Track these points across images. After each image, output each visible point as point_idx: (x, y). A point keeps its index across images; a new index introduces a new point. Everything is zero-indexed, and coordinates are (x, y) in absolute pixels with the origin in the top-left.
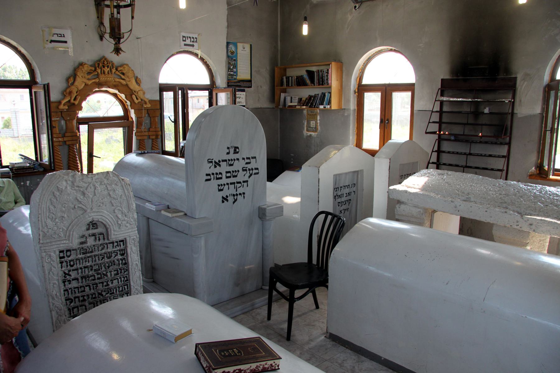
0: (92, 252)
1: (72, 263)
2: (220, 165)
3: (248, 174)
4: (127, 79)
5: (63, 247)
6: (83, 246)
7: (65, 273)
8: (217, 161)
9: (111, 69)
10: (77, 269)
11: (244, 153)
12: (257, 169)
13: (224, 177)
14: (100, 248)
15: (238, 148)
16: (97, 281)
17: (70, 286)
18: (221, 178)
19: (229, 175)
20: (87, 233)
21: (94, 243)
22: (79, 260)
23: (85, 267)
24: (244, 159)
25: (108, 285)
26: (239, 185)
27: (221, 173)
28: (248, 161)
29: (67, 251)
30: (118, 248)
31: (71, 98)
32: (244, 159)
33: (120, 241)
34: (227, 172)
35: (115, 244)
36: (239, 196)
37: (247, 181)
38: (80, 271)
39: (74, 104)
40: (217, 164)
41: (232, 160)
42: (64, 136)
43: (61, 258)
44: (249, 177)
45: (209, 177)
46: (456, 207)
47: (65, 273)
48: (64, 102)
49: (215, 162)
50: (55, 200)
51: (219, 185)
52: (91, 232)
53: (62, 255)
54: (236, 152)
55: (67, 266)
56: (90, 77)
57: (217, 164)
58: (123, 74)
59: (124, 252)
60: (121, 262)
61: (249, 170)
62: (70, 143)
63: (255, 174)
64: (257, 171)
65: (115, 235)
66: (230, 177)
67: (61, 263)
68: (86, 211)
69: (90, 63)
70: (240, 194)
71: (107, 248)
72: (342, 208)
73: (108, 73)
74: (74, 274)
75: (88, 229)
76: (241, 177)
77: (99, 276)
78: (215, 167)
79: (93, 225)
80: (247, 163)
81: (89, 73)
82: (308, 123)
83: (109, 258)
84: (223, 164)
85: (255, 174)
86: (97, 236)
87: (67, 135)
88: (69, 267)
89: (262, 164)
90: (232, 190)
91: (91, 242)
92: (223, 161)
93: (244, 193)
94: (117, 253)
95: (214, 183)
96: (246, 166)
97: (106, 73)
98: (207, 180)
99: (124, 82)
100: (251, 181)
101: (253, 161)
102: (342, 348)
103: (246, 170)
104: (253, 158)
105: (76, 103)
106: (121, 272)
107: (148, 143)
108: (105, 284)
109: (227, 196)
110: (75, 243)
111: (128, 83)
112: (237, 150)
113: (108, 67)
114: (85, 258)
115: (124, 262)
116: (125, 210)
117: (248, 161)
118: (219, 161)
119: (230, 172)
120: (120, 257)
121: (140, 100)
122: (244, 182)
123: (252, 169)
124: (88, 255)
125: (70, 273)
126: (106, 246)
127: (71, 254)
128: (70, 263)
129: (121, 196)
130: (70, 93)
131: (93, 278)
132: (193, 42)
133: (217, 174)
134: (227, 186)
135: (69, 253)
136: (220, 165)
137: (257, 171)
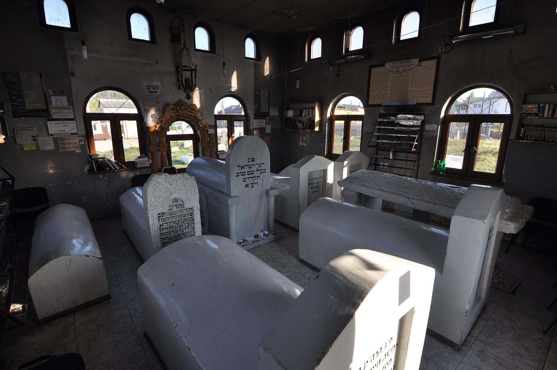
3: (260, 172)
10: (167, 223)
13: (246, 174)
20: (172, 204)
40: (243, 167)
42: (159, 146)
52: (175, 204)
54: (253, 161)
56: (174, 111)
57: (243, 167)
58: (193, 110)
59: (192, 214)
65: (188, 205)
68: (172, 193)
69: (174, 103)
74: (165, 226)
76: (256, 174)
79: (176, 200)
81: (173, 110)
82: (302, 139)
89: (267, 166)
91: (175, 209)
95: (241, 178)
100: (261, 176)
102: (305, 267)
105: (165, 127)
107: (208, 151)
110: (166, 210)
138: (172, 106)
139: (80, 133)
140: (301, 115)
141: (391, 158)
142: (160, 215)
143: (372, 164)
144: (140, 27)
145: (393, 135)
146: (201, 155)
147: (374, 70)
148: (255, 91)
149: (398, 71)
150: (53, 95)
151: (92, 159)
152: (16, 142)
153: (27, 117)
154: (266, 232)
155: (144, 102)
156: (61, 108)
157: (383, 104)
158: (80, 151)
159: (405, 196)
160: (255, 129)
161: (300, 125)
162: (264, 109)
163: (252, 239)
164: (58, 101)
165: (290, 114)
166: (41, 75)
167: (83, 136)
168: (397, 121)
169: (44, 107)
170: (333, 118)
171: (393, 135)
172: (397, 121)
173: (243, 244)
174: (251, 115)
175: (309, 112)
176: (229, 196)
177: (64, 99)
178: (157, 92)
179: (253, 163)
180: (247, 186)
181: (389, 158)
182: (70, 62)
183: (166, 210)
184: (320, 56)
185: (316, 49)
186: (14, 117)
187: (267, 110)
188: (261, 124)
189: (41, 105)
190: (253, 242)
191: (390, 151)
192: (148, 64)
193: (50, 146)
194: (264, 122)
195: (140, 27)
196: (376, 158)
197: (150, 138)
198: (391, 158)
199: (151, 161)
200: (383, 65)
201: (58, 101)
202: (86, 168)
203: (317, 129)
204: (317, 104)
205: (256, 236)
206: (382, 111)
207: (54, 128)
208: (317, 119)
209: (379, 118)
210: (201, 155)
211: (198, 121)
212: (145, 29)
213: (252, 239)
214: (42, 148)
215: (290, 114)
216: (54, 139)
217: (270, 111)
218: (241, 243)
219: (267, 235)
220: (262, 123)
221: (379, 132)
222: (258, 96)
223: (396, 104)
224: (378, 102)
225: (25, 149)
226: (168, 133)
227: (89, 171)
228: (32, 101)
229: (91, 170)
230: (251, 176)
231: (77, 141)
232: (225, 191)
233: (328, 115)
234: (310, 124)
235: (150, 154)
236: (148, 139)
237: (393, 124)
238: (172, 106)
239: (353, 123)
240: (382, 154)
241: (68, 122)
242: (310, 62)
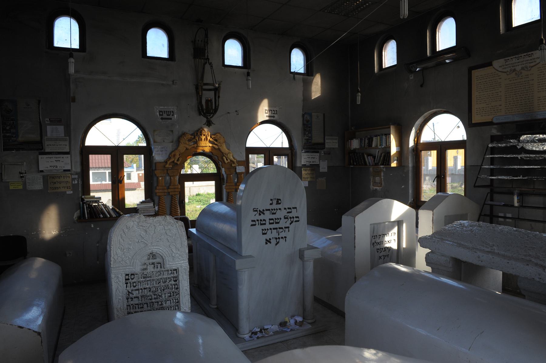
0: (150, 277)
1: (135, 285)
2: (264, 214)
3: (289, 221)
10: (138, 290)
11: (286, 204)
12: (298, 217)
13: (267, 223)
15: (280, 200)
16: (153, 300)
17: (132, 302)
18: (265, 224)
20: (147, 262)
21: (152, 270)
23: (144, 289)
24: (285, 209)
25: (162, 304)
27: (264, 220)
28: (290, 210)
29: (132, 275)
32: (285, 209)
34: (270, 219)
37: (288, 227)
38: (141, 291)
39: (177, 164)
42: (168, 188)
43: (126, 280)
44: (290, 224)
45: (254, 223)
46: (479, 257)
51: (263, 230)
52: (151, 261)
53: (127, 277)
54: (278, 203)
57: (262, 212)
59: (176, 279)
60: (174, 287)
61: (291, 218)
62: (173, 193)
63: (296, 221)
64: (297, 219)
66: (273, 223)
67: (127, 283)
69: (191, 133)
70: (282, 238)
72: (381, 254)
74: (135, 293)
75: (149, 259)
76: (283, 224)
77: (156, 296)
78: (260, 215)
79: (153, 255)
80: (288, 212)
85: (296, 221)
87: (170, 187)
91: (150, 268)
92: (267, 210)
93: (285, 237)
95: (259, 228)
96: (288, 214)
98: (252, 225)
100: (292, 227)
101: (293, 210)
103: (287, 218)
104: (293, 208)
105: (178, 163)
106: (173, 295)
108: (160, 303)
109: (270, 239)
111: (220, 147)
112: (280, 202)
115: (176, 287)
117: (290, 210)
118: (263, 210)
119: (272, 219)
120: (173, 283)
121: (229, 161)
122: (285, 228)
123: (293, 218)
130: (174, 155)
131: (150, 297)
132: (274, 114)
133: (261, 220)
135: (132, 277)
136: (264, 214)
137: (297, 219)
138: (190, 136)
139: (73, 169)
140: (370, 145)
141: (516, 204)
142: (129, 277)
143: (485, 215)
144: (157, 44)
145: (516, 167)
146: (225, 200)
147: (476, 73)
148: (303, 115)
149: (515, 70)
150: (50, 125)
151: (83, 203)
152: (2, 180)
153: (18, 149)
154: (299, 319)
155: (154, 131)
156: (56, 139)
157: (495, 121)
158: (72, 192)
159: (536, 265)
160: (304, 166)
161: (369, 160)
162: (317, 138)
163: (275, 328)
164: (54, 131)
165: (355, 144)
166: (39, 101)
167: (77, 174)
168: (521, 145)
169: (38, 139)
170: (420, 147)
171: (516, 167)
172: (521, 145)
173: (259, 335)
174: (298, 146)
175: (381, 140)
176: (238, 254)
177: (61, 128)
178: (171, 119)
180: (268, 241)
181: (513, 206)
182: (72, 86)
183: (137, 269)
184: (395, 63)
185: (390, 56)
186: (5, 150)
187: (321, 141)
188: (313, 160)
189: (35, 137)
190: (276, 333)
191: (512, 194)
192: (162, 84)
193: (39, 186)
194: (318, 157)
195: (157, 44)
196: (492, 206)
197: (158, 178)
198: (516, 204)
199: (157, 208)
200: (490, 64)
201: (54, 131)
202: (76, 215)
203: (394, 164)
204: (392, 130)
205: (283, 324)
206: (494, 131)
207: (46, 163)
208: (394, 149)
209: (489, 142)
210: (225, 200)
211: (223, 154)
212: (163, 45)
213: (275, 328)
214: (30, 187)
215: (355, 144)
216: (44, 177)
217: (326, 141)
218: (255, 333)
219: (301, 324)
220: (315, 158)
221: (492, 164)
222: (308, 121)
223: (517, 119)
224: (487, 119)
225: (11, 188)
226: (183, 172)
227: (79, 218)
228: (26, 131)
229: (81, 218)
230: (275, 226)
231: (69, 180)
232: (236, 249)
233: (411, 143)
234: (385, 156)
235: (156, 199)
236: (155, 179)
237: (513, 149)
238: (190, 136)
239: (451, 154)
240: (500, 200)
241: (62, 156)
242: (382, 72)
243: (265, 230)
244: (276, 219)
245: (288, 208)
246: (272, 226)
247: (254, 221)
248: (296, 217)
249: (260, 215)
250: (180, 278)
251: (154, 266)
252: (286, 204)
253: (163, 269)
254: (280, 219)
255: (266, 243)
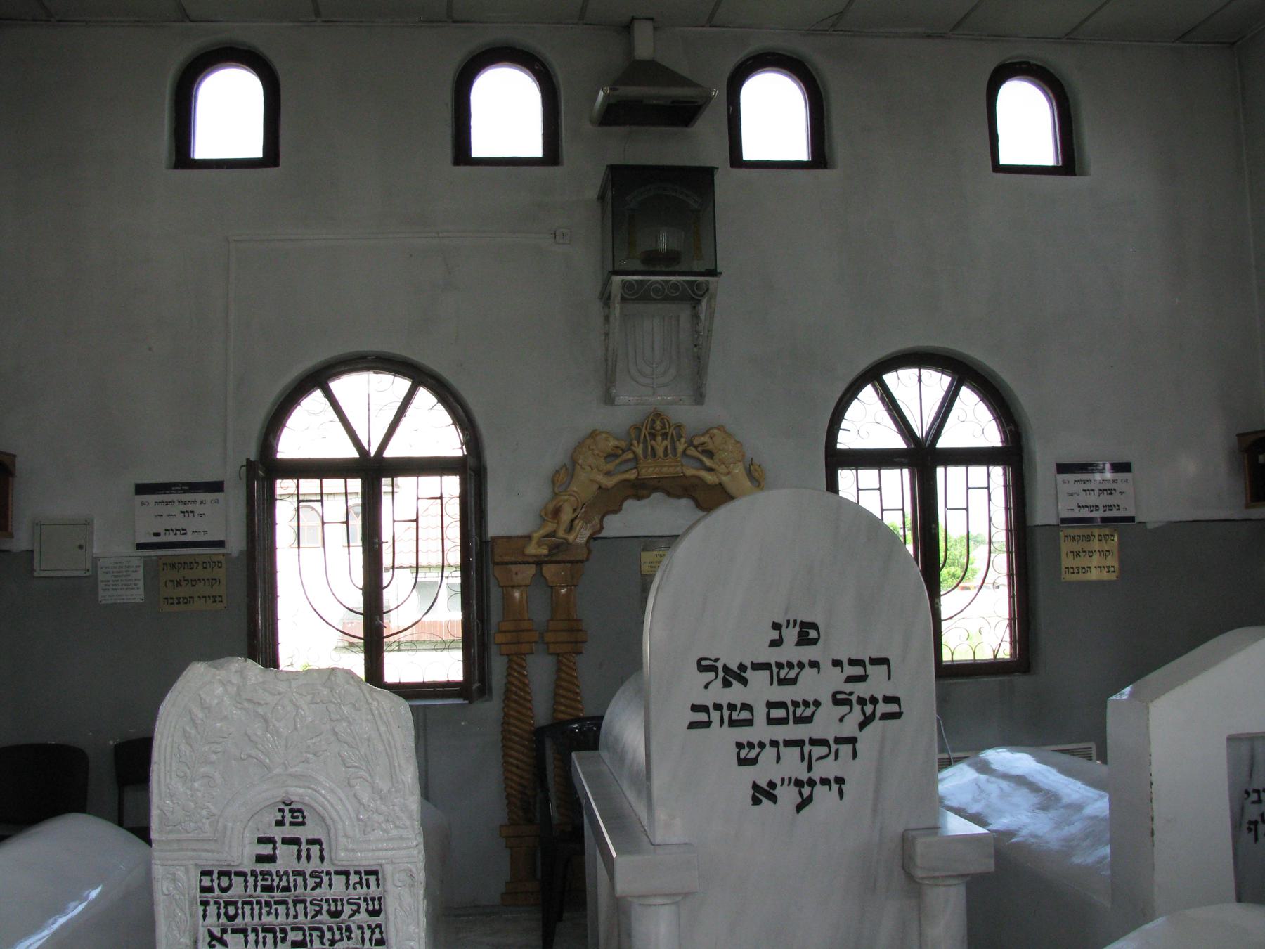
1: (231, 911)
2: (744, 682)
3: (856, 715)
4: (722, 469)
5: (212, 860)
6: (266, 867)
7: (211, 934)
8: (734, 667)
9: (673, 442)
11: (841, 641)
12: (895, 700)
14: (311, 882)
15: (814, 626)
18: (749, 723)
19: (778, 713)
22: (250, 903)
23: (265, 930)
24: (837, 663)
26: (819, 751)
27: (746, 707)
28: (858, 671)
29: (221, 874)
30: (362, 892)
31: (558, 527)
32: (837, 663)
33: (368, 873)
34: (771, 705)
35: (354, 879)
36: (820, 790)
37: (852, 741)
41: (790, 665)
43: (204, 890)
44: (862, 726)
45: (702, 717)
47: (211, 934)
48: (536, 536)
49: (725, 668)
50: (193, 732)
51: (740, 746)
52: (289, 832)
53: (206, 882)
54: (804, 640)
55: (219, 916)
56: (610, 467)
57: (735, 676)
58: (710, 454)
61: (861, 701)
63: (885, 716)
64: (893, 708)
66: (784, 721)
67: (205, 903)
70: (825, 782)
71: (330, 886)
73: (666, 454)
76: (827, 723)
78: (727, 684)
79: (294, 813)
80: (850, 679)
81: (611, 456)
83: (335, 914)
84: (758, 679)
85: (885, 716)
86: (304, 847)
88: (223, 920)
90: (791, 763)
92: (757, 666)
93: (840, 781)
94: (359, 905)
95: (723, 738)
96: (849, 687)
97: (660, 451)
98: (692, 725)
99: (710, 478)
100: (867, 738)
101: (876, 672)
103: (847, 702)
104: (874, 661)
109: (772, 785)
111: (725, 479)
112: (813, 634)
113: (665, 436)
114: (268, 904)
115: (377, 936)
116: (384, 785)
117: (858, 671)
119: (782, 705)
120: (362, 917)
122: (839, 741)
123: (874, 701)
124: (278, 895)
125: (225, 937)
126: (326, 879)
127: (230, 886)
128: (226, 908)
129: (369, 740)
130: (557, 512)
133: (732, 707)
134: (770, 752)
135: (225, 882)
136: (744, 682)
137: (893, 708)
138: (612, 443)
179: (807, 654)
180: (763, 793)
183: (242, 854)
210: (1094, 757)
230: (801, 732)
243: (751, 745)
244: (796, 704)
245: (852, 662)
246: (781, 733)
247: (704, 709)
248: (888, 700)
249: (727, 684)
250: (391, 905)
251: (299, 851)
252: (841, 641)
253: (326, 866)
254: (817, 704)
255: (756, 801)
